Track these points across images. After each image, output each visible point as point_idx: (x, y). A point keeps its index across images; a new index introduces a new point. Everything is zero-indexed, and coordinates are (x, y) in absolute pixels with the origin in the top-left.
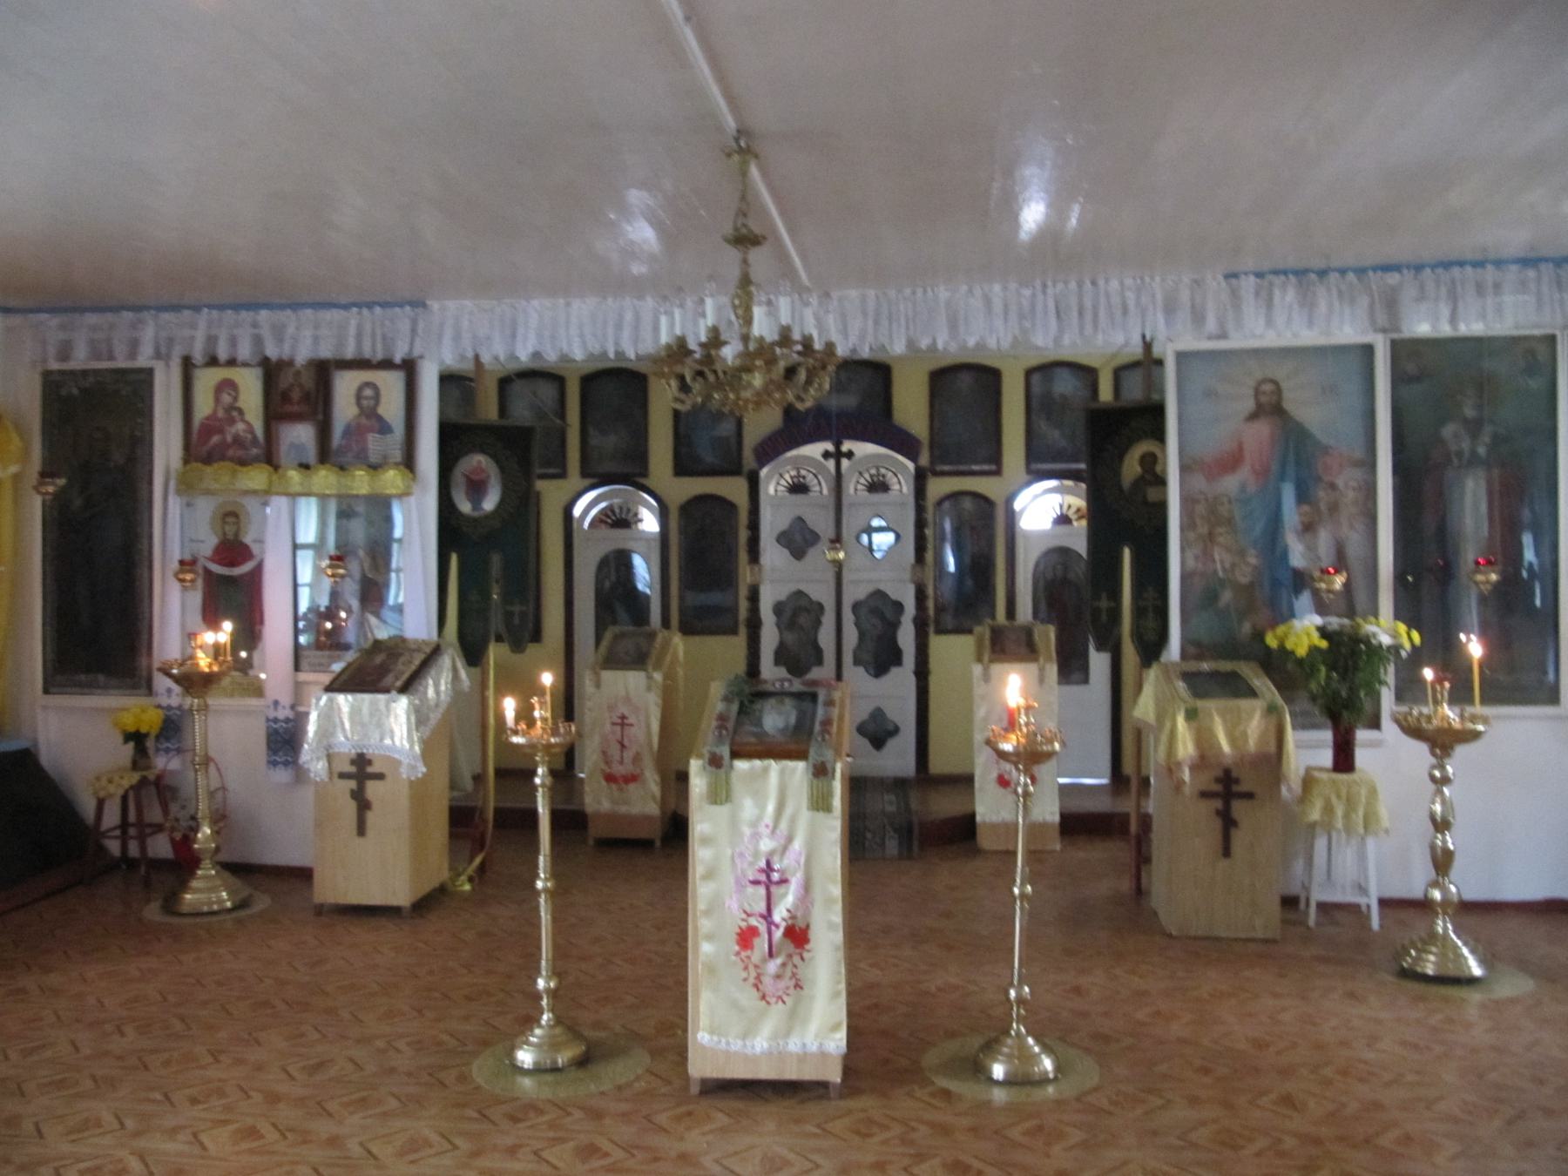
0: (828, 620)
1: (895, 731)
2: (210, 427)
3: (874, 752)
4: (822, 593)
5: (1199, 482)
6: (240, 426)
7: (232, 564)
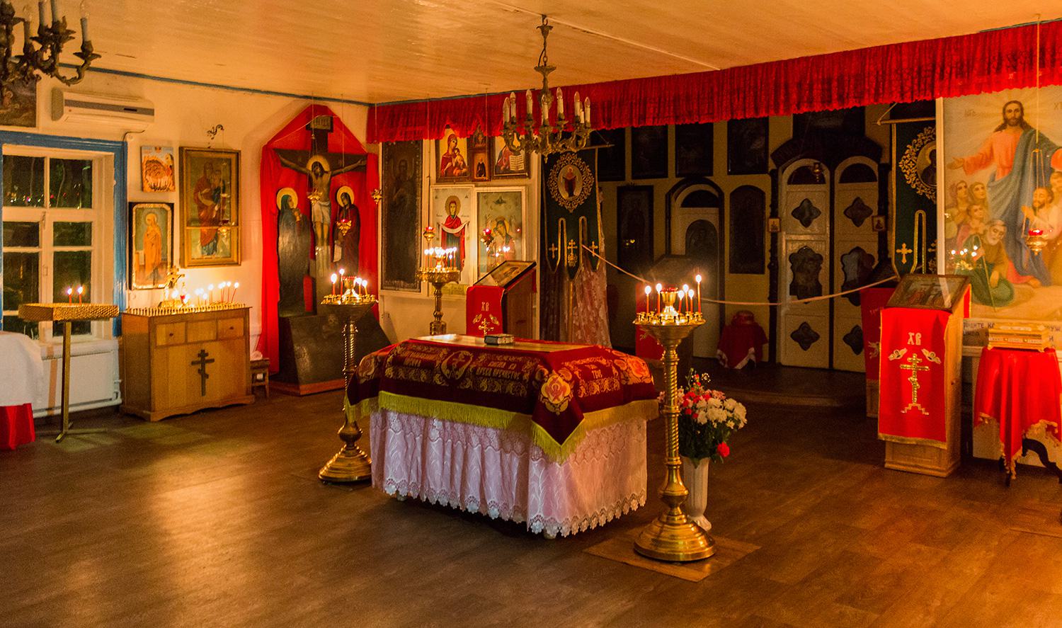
0: (825, 265)
2: (447, 159)
4: (822, 249)
5: (959, 174)
6: (458, 157)
7: (453, 228)
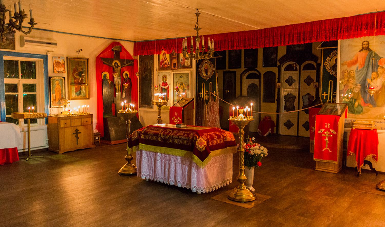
0: (297, 99)
1: (293, 125)
2: (162, 61)
3: (306, 131)
5: (345, 67)
